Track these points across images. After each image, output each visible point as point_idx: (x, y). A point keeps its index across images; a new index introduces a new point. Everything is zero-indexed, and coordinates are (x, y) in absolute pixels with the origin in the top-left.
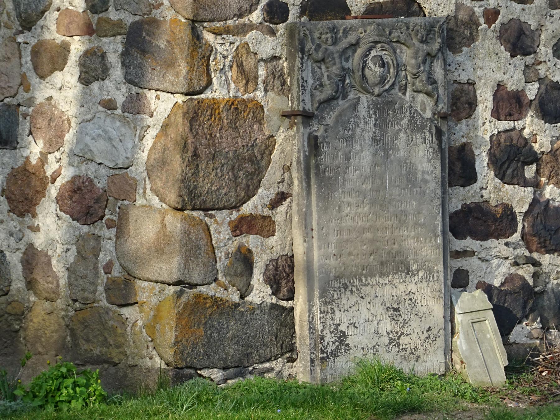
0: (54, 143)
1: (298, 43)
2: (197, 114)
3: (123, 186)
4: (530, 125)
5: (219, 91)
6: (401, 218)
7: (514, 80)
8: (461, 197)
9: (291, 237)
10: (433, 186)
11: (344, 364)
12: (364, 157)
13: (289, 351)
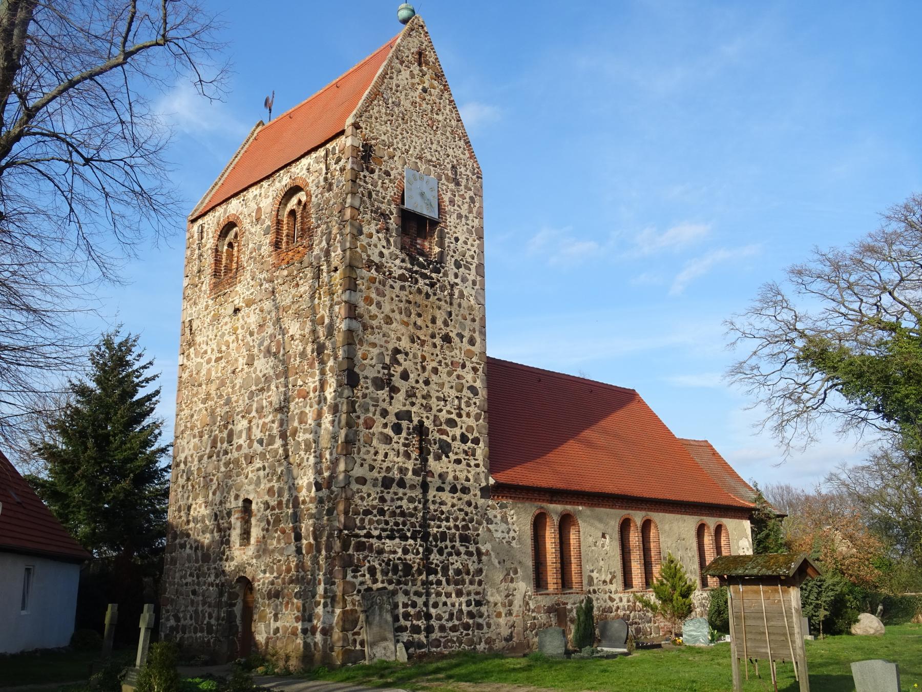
0: (319, 620)
1: (363, 597)
2: (344, 613)
3: (331, 628)
4: (410, 609)
5: (348, 608)
6: (385, 630)
7: (406, 601)
8: (397, 625)
9: (364, 636)
10: (391, 623)
11: (375, 660)
12: (377, 618)
13: (364, 658)
